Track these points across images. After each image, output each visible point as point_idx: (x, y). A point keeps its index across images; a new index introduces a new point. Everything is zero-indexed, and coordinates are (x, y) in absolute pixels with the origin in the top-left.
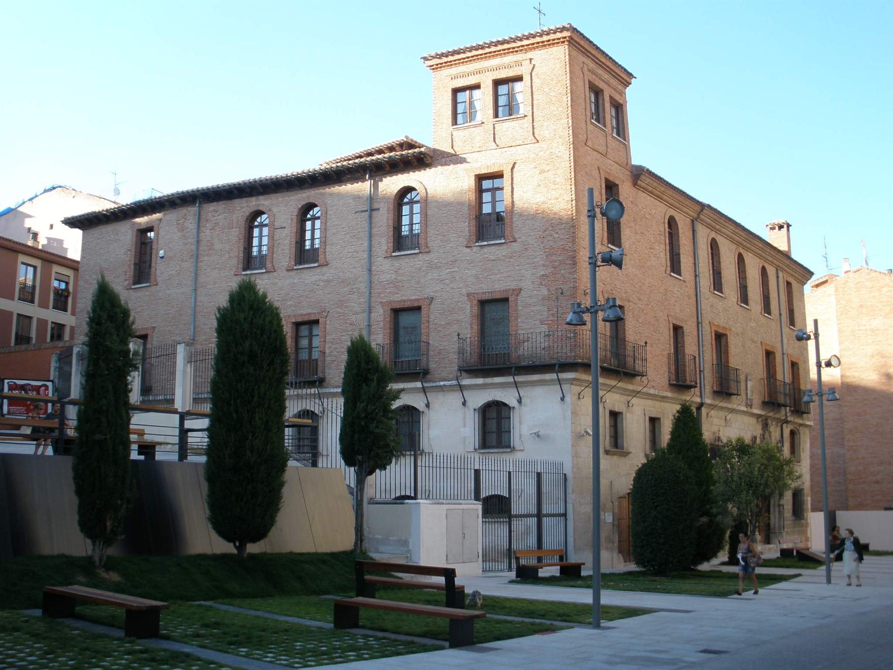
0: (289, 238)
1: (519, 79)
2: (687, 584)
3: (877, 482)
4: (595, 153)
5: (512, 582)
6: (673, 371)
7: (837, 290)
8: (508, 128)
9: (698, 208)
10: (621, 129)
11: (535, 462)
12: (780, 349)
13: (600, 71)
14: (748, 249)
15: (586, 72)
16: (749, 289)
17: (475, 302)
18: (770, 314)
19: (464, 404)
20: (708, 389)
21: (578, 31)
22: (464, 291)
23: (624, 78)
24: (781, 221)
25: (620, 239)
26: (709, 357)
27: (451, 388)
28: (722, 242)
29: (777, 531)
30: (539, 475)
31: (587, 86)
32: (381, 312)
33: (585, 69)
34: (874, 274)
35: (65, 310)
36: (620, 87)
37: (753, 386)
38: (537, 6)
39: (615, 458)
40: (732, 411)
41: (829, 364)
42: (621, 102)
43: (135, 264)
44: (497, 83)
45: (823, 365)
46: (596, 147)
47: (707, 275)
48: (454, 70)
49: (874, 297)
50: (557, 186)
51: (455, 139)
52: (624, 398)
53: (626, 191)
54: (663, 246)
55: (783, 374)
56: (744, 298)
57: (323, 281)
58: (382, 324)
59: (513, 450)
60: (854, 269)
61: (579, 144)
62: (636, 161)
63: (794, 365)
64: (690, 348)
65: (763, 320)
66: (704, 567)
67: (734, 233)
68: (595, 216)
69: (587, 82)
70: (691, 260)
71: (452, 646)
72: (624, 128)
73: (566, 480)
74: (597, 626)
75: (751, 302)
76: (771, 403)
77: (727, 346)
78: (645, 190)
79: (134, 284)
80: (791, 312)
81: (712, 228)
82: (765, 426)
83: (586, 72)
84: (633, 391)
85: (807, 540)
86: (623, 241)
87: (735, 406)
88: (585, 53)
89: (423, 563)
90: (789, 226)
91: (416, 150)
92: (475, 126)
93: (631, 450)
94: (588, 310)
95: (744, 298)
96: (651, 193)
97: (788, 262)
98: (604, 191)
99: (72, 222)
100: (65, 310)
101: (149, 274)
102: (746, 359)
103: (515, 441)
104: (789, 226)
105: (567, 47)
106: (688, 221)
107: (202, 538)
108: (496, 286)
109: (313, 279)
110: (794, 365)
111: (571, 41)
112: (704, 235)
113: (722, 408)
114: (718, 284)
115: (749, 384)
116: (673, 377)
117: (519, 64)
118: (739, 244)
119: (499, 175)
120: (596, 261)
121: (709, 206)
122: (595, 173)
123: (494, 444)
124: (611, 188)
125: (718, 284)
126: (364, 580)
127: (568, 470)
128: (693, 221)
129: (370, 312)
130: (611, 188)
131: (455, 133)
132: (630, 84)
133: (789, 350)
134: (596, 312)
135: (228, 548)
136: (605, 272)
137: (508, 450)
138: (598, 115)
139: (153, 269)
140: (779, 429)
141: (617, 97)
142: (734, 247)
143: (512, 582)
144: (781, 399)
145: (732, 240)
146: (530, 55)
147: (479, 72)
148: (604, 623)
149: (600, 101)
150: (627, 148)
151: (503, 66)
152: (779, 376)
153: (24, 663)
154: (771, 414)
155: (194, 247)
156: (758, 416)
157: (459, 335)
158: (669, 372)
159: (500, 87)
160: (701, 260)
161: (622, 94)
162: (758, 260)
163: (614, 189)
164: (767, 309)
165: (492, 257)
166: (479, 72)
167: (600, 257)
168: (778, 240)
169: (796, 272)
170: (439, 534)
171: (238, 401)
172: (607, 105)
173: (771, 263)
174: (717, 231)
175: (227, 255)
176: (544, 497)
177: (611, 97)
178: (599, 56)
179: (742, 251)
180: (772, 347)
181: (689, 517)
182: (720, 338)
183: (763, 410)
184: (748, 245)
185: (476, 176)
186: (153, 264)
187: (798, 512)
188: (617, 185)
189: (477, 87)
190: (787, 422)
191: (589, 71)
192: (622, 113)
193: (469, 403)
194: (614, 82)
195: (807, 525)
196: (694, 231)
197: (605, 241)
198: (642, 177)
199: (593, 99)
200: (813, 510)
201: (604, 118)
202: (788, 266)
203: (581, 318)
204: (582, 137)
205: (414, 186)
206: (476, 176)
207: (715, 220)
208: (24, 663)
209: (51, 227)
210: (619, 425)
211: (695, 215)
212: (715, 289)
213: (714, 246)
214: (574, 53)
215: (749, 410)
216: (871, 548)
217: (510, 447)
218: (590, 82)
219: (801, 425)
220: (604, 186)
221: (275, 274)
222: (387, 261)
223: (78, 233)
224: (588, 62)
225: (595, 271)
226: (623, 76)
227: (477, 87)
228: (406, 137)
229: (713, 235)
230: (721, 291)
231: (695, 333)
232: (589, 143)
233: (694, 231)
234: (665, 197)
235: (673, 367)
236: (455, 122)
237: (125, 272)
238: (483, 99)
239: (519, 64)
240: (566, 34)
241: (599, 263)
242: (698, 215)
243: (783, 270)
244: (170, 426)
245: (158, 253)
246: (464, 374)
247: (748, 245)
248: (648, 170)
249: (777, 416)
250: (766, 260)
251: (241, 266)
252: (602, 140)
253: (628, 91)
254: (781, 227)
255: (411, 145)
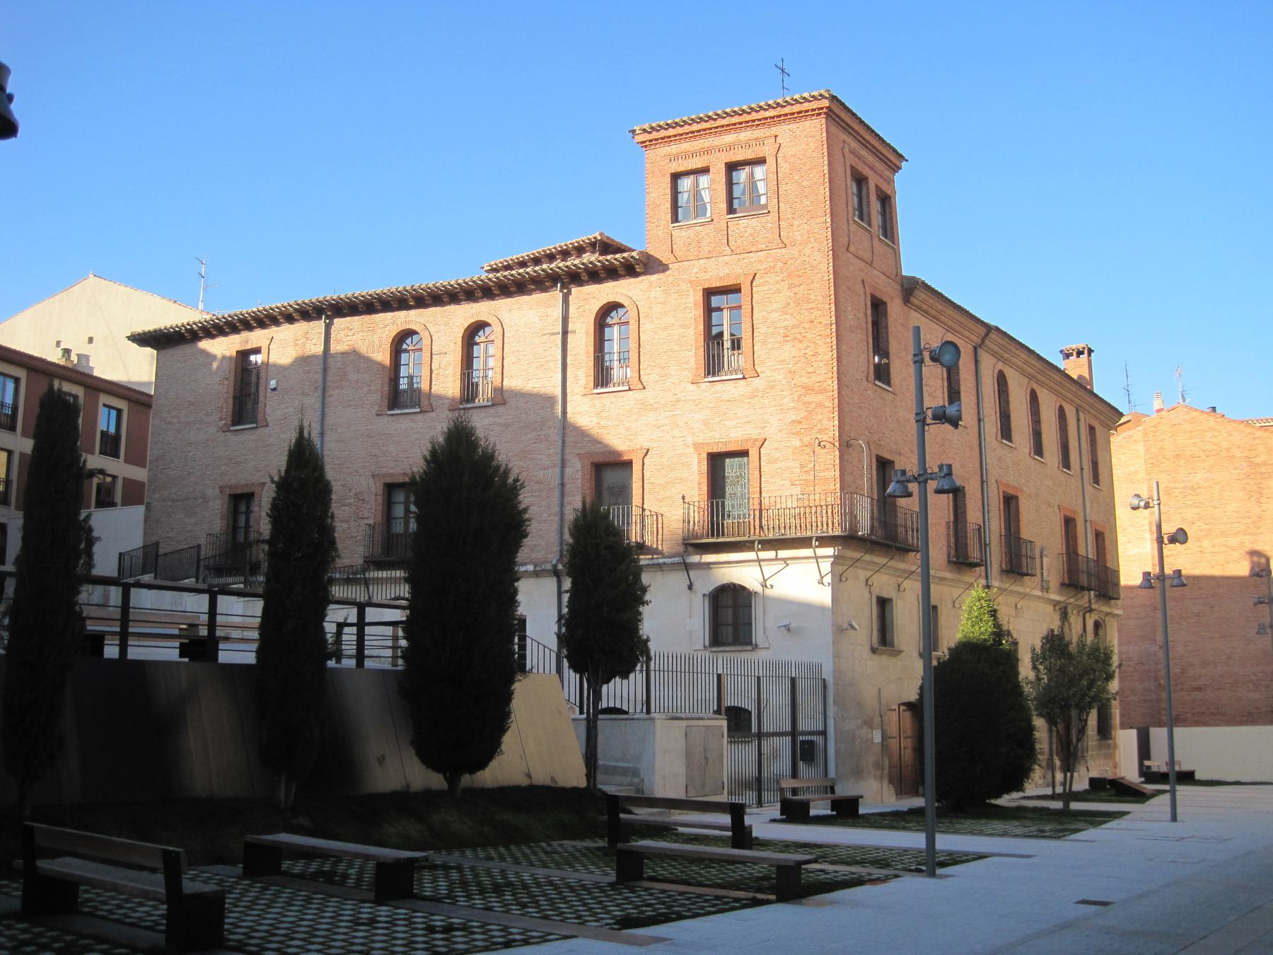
0: (451, 367)
1: (761, 161)
2: (981, 824)
3: (1199, 689)
4: (859, 262)
5: (773, 821)
6: (952, 545)
7: (1145, 434)
8: (744, 226)
9: (982, 331)
10: (889, 229)
11: (788, 664)
12: (1082, 514)
13: (864, 153)
14: (1042, 384)
15: (847, 154)
16: (1044, 436)
17: (705, 455)
18: (1069, 468)
19: (690, 587)
20: (995, 569)
21: (839, 101)
22: (690, 441)
23: (892, 160)
24: (1081, 345)
25: (889, 373)
26: (996, 526)
27: (673, 567)
28: (1011, 375)
29: (1103, 752)
30: (793, 680)
31: (849, 172)
32: (579, 466)
33: (846, 149)
34: (1195, 414)
35: (117, 456)
36: (888, 173)
37: (1051, 565)
38: (780, 64)
39: (884, 658)
40: (1024, 596)
41: (1173, 540)
42: (889, 192)
43: (234, 397)
44: (732, 167)
45: (1166, 541)
46: (861, 253)
47: (993, 418)
48: (674, 149)
49: (1195, 444)
50: (812, 305)
51: (677, 241)
52: (893, 581)
53: (895, 308)
54: (940, 382)
55: (1086, 548)
56: (1038, 449)
57: (499, 425)
58: (579, 483)
59: (756, 647)
60: (1169, 407)
61: (840, 249)
62: (906, 272)
63: (1099, 536)
64: (973, 516)
65: (1061, 477)
66: (1005, 801)
67: (1026, 363)
68: (922, 361)
69: (848, 168)
70: (974, 399)
71: (779, 900)
72: (892, 228)
73: (825, 687)
74: (932, 874)
75: (1046, 453)
76: (1072, 583)
77: (1017, 512)
78: (918, 309)
79: (233, 425)
80: (1095, 465)
81: (999, 358)
82: (1064, 615)
83: (847, 154)
84: (905, 571)
85: (1115, 766)
86: (892, 376)
87: (1028, 590)
88: (846, 128)
89: (660, 792)
90: (1090, 351)
91: (625, 255)
92: (702, 224)
93: (902, 648)
94: (915, 479)
95: (1038, 449)
96: (920, 309)
97: (1091, 400)
98: (869, 312)
99: (143, 339)
100: (117, 456)
101: (255, 411)
102: (1040, 529)
103: (758, 635)
104: (1090, 351)
105: (824, 121)
106: (970, 347)
107: (396, 768)
108: (727, 436)
109: (486, 421)
110: (1099, 536)
111: (831, 115)
112: (989, 367)
113: (1012, 592)
114: (1006, 432)
115: (1045, 559)
116: (953, 552)
117: (760, 141)
118: (1031, 378)
119: (735, 289)
120: (925, 418)
121: (998, 329)
122: (859, 287)
123: (730, 640)
124: (878, 306)
125: (1006, 432)
126: (620, 819)
127: (827, 674)
128: (975, 348)
129: (563, 467)
130: (878, 306)
131: (676, 233)
132: (900, 168)
133: (1091, 515)
134: (926, 482)
135: (437, 781)
136: (936, 432)
137: (750, 648)
138: (862, 212)
139: (261, 405)
140: (1081, 619)
141: (884, 187)
142: (1025, 381)
143: (773, 821)
144: (1084, 580)
145: (1023, 373)
146: (774, 130)
147: (707, 151)
148: (939, 871)
149: (864, 193)
150: (896, 254)
151: (738, 143)
152: (1081, 551)
153: (35, 930)
154: (1072, 600)
155: (319, 377)
156: (1056, 603)
157: (683, 498)
158: (949, 546)
159: (734, 174)
160: (985, 399)
161: (890, 182)
162: (1055, 398)
163: (881, 307)
164: (1066, 463)
165: (726, 397)
166: (707, 151)
167: (929, 413)
168: (1074, 368)
169: (1101, 412)
170: (667, 755)
171: (82, 546)
172: (873, 197)
173: (1071, 402)
174: (1005, 361)
175: (366, 389)
176: (799, 708)
177: (877, 186)
178: (863, 132)
179: (1035, 386)
180: (1074, 512)
181: (982, 739)
182: (1010, 502)
183: (1061, 594)
184: (1043, 379)
185: (704, 290)
186: (261, 399)
187: (1104, 730)
188: (885, 303)
189: (705, 170)
190: (1091, 611)
191: (851, 152)
192: (890, 207)
193: (696, 586)
194: (879, 166)
195: (1115, 746)
196: (976, 361)
197: (872, 376)
198: (917, 292)
199: (855, 190)
200: (1123, 726)
201: (869, 215)
202: (1091, 406)
203: (906, 488)
204: (843, 241)
205: (621, 301)
206: (704, 290)
207: (1002, 347)
208: (35, 930)
209: (91, 340)
210: (887, 614)
211: (979, 341)
212: (1002, 437)
213: (1002, 380)
214: (834, 129)
215: (1046, 595)
216: (1198, 776)
217: (750, 643)
218: (852, 167)
219: (1108, 614)
220: (869, 304)
221: (433, 414)
222: (585, 399)
223: (149, 352)
224: (849, 140)
225: (924, 431)
226: (892, 158)
227: (705, 170)
228: (601, 234)
229: (1000, 366)
230: (1009, 438)
231: (979, 494)
232: (852, 249)
233: (976, 361)
234: (943, 318)
235: (952, 540)
236: (675, 219)
237: (221, 409)
238: (711, 187)
239: (760, 141)
240: (826, 103)
241: (929, 421)
242: (983, 341)
243: (1085, 410)
244: (371, 625)
245: (267, 383)
246: (690, 549)
247: (1043, 379)
248: (923, 283)
249: (1080, 603)
250: (1064, 398)
251: (385, 403)
252: (867, 243)
253: (897, 177)
254: (1080, 353)
255: (606, 247)
